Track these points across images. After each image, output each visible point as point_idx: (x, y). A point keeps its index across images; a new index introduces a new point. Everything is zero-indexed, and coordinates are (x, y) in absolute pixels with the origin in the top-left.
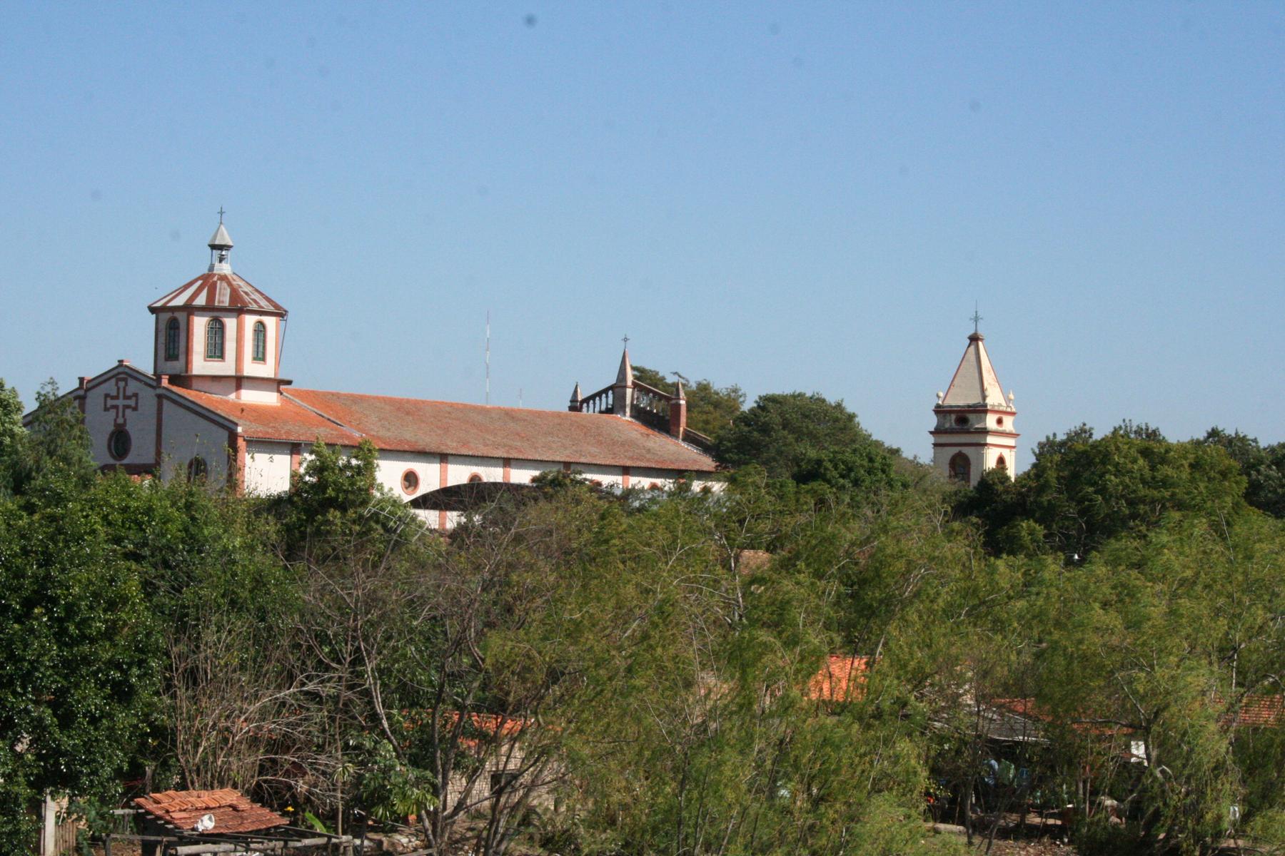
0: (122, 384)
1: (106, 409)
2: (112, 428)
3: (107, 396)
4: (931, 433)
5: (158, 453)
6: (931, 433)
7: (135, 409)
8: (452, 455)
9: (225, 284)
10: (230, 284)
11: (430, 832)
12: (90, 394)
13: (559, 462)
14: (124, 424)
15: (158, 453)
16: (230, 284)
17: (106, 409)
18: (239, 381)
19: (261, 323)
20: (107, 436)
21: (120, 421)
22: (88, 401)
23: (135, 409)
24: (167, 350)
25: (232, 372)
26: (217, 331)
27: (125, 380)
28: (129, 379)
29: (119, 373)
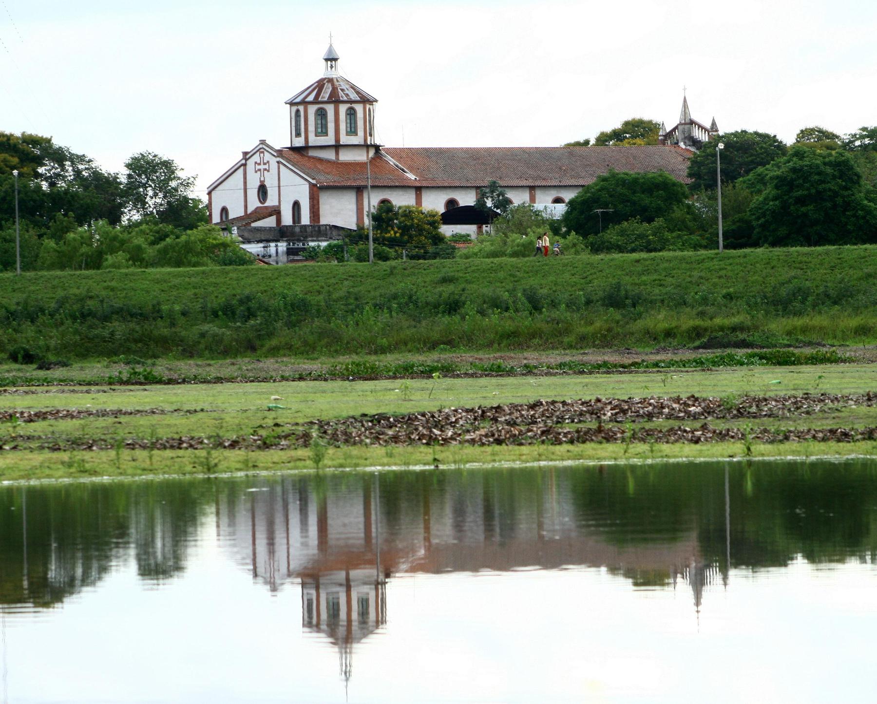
0: (262, 155)
1: (256, 172)
2: (258, 184)
3: (256, 163)
4: (376, 101)
5: (279, 202)
6: (376, 101)
7: (268, 171)
8: (427, 187)
9: (330, 85)
10: (333, 85)
11: (749, 351)
12: (248, 162)
13: (526, 186)
14: (264, 181)
15: (279, 202)
16: (333, 85)
17: (256, 172)
18: (337, 147)
19: (351, 109)
20: (257, 190)
21: (262, 179)
22: (248, 167)
23: (268, 171)
24: (296, 130)
25: (333, 142)
26: (322, 114)
27: (263, 152)
28: (265, 152)
29: (260, 149)
